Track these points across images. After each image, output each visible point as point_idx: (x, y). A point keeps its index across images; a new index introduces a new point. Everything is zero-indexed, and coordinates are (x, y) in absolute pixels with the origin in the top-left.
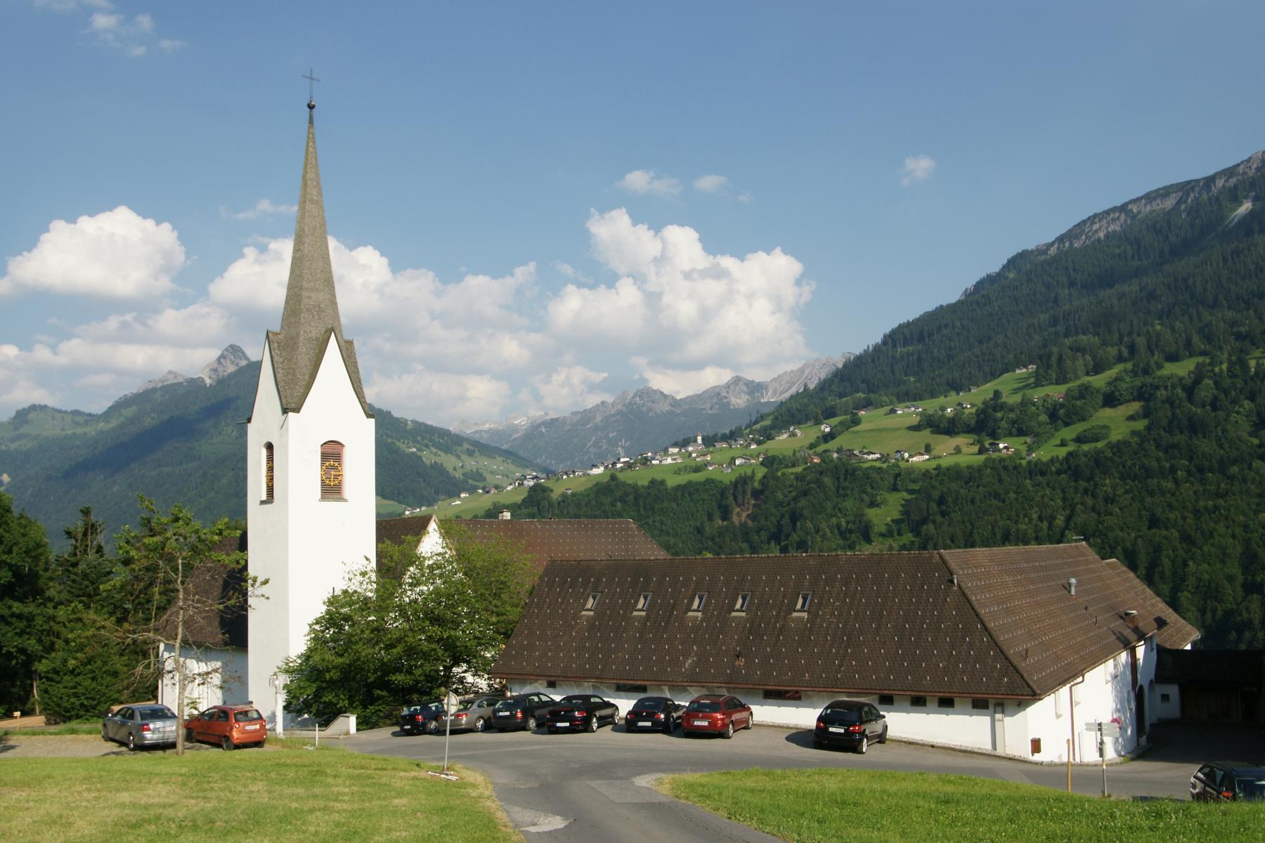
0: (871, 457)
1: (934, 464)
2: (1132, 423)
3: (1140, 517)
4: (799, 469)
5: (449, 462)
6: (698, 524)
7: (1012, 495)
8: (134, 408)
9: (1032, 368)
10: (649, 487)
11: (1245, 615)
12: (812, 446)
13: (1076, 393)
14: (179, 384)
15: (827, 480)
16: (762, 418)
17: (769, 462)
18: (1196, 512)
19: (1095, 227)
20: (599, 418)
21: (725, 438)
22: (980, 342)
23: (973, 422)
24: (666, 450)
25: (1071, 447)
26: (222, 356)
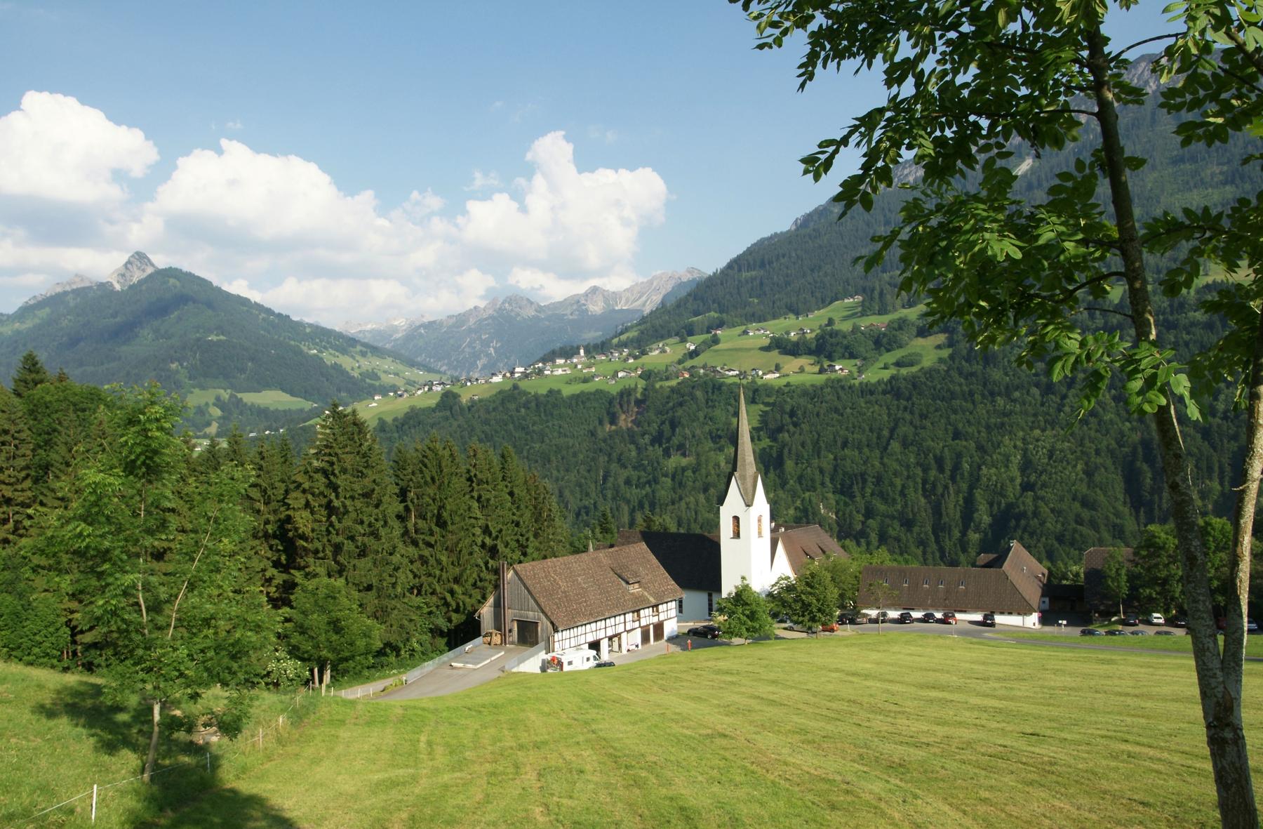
0: (731, 373)
1: (784, 381)
2: (939, 351)
3: (946, 430)
4: (673, 383)
5: (346, 362)
6: (591, 427)
7: (848, 410)
8: (47, 310)
9: (859, 298)
10: (547, 396)
11: (1022, 508)
12: (680, 362)
13: (896, 325)
14: (90, 288)
15: (699, 394)
16: (626, 330)
17: (647, 375)
18: (988, 427)
19: (906, 172)
20: (472, 321)
22: (812, 270)
23: (813, 346)
24: (554, 362)
25: (893, 371)
26: (129, 262)
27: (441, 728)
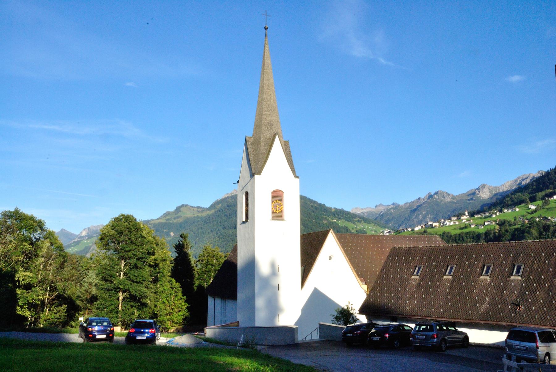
21: (478, 212)
24: (450, 219)
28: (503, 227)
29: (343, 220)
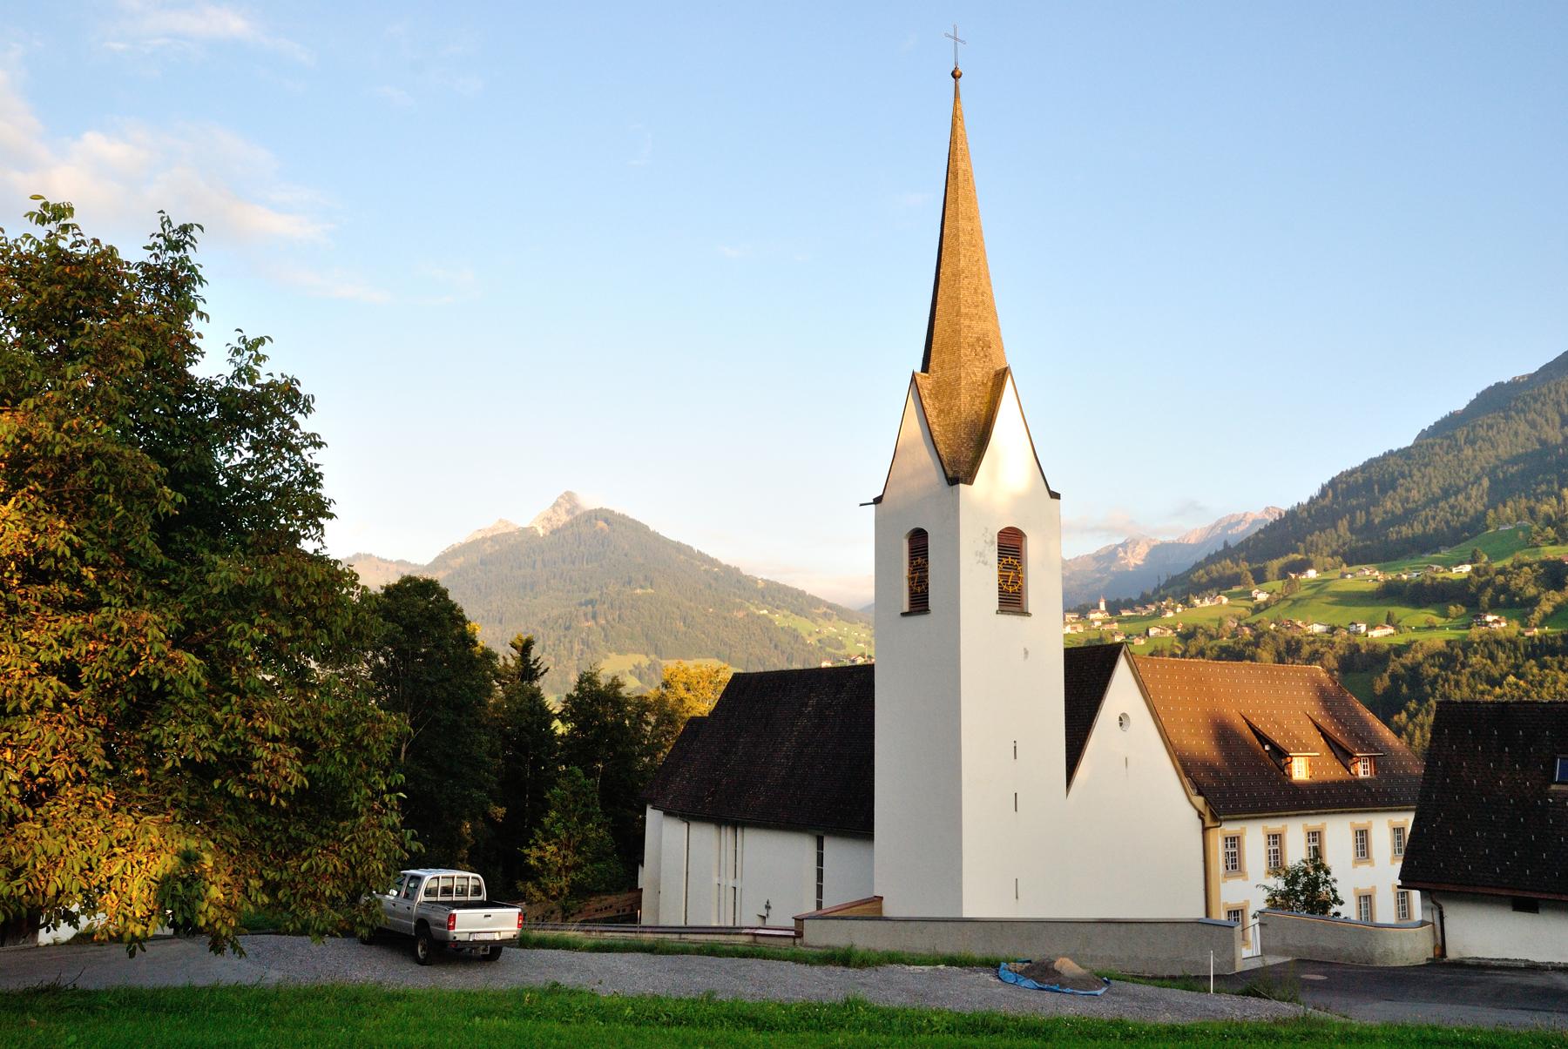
5: (803, 625)
14: (510, 534)
21: (1129, 605)
27: (1473, 660)
28: (1191, 642)
29: (787, 613)
